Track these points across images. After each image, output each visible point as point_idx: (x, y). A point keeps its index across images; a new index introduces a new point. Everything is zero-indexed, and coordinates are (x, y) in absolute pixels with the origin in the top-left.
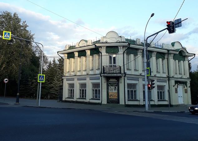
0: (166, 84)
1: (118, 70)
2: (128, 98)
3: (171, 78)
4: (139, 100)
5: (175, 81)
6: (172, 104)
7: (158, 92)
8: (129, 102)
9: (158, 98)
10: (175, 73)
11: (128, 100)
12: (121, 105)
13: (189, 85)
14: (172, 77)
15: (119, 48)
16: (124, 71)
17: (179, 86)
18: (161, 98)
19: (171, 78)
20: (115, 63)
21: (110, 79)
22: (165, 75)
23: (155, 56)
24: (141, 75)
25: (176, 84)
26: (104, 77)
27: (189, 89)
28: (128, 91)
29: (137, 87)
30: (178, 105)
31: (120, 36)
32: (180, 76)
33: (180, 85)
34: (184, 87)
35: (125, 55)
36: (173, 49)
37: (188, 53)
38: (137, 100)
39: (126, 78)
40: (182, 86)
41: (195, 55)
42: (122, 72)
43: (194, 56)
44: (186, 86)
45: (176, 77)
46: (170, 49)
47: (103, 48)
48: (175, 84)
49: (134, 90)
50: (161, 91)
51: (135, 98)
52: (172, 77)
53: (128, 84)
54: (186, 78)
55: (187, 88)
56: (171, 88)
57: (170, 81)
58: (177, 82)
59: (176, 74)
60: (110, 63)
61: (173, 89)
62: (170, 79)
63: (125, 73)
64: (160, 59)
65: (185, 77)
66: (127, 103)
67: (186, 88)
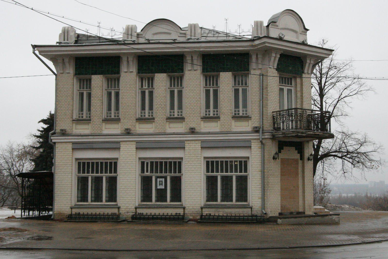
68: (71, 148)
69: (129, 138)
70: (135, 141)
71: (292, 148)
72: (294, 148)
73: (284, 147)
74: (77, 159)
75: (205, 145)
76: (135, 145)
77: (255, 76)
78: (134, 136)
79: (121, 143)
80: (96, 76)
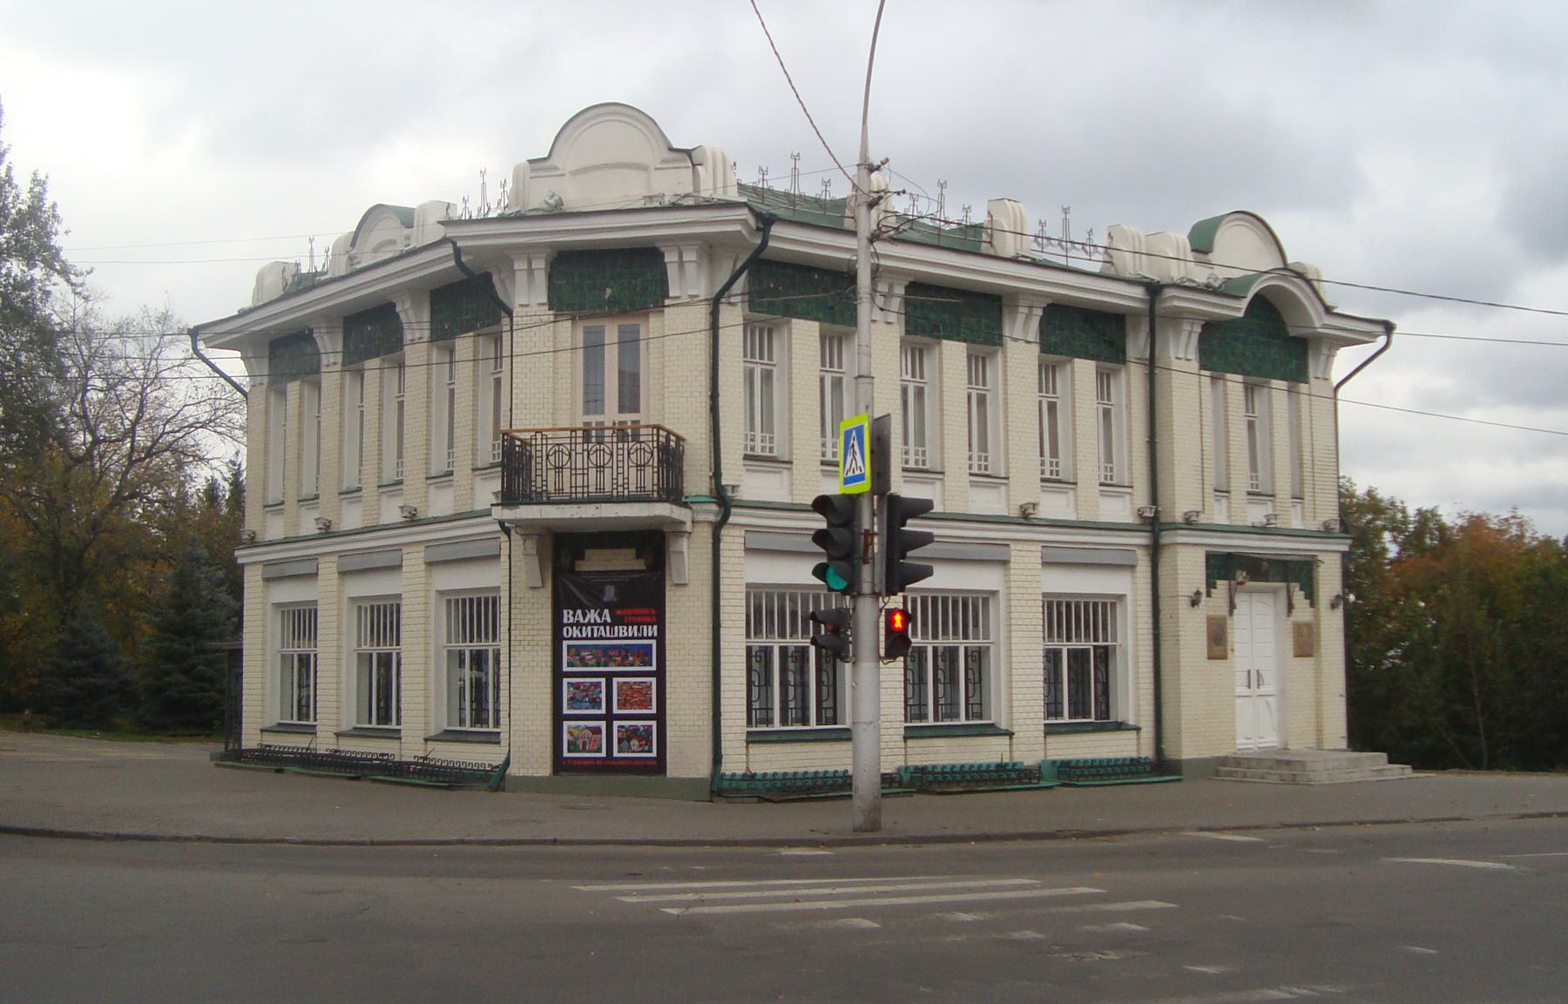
0: (1130, 588)
1: (640, 467)
2: (1049, 714)
3: (1174, 527)
4: (1003, 726)
5: (1210, 557)
6: (1170, 753)
7: (1052, 657)
8: (755, 749)
9: (1053, 709)
10: (1209, 490)
11: (753, 739)
12: (679, 781)
13: (1329, 579)
14: (1179, 518)
15: (670, 258)
16: (717, 474)
17: (1240, 600)
18: (1079, 708)
19: (1174, 527)
20: (630, 398)
21: (581, 556)
22: (1120, 510)
23: (896, 304)
24: (1026, 518)
25: (1222, 584)
26: (525, 537)
27: (1332, 628)
28: (757, 660)
29: (997, 612)
30: (1224, 761)
31: (688, 153)
32: (1256, 514)
33: (1250, 592)
34: (1290, 607)
35: (733, 317)
36: (1201, 275)
37: (1328, 310)
38: (992, 731)
39: (732, 541)
40: (1269, 599)
41: (1388, 328)
42: (696, 481)
43: (1382, 340)
44: (1311, 596)
45: (1221, 519)
46: (1175, 272)
47: (520, 265)
48: (1210, 585)
49: (972, 642)
50: (951, 642)
51: (977, 707)
52: (1179, 518)
53: (1050, 605)
54: (1314, 526)
55: (1317, 616)
56: (1174, 617)
57: (1165, 558)
58: (1222, 566)
59: (1223, 491)
60: (593, 401)
61: (1190, 629)
62: (1166, 538)
63: (723, 499)
64: (797, 323)
65: (1296, 524)
66: (733, 765)
67: (1303, 611)
68: (259, 578)
69: (323, 546)
70: (336, 552)
71: (626, 551)
72: (633, 551)
73: (588, 553)
74: (353, 599)
75: (274, 571)
76: (422, 554)
77: (465, 364)
78: (336, 540)
79: (405, 550)
80: (801, 321)
